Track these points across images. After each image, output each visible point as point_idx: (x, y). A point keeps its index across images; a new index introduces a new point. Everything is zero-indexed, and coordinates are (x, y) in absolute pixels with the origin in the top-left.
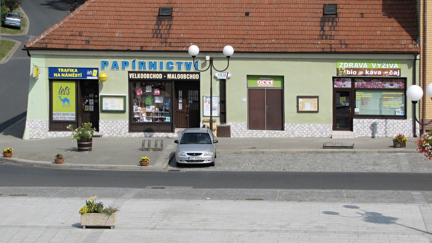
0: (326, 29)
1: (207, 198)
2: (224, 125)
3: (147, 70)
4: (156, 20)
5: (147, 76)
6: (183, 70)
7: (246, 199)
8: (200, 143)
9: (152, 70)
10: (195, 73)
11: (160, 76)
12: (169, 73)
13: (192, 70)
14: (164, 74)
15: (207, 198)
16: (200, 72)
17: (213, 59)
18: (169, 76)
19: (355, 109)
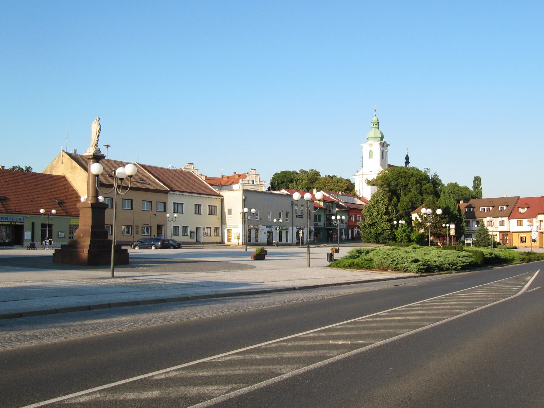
0: (249, 248)
1: (350, 230)
2: (33, 243)
3: (4, 220)
4: (306, 250)
5: (4, 223)
6: (19, 220)
7: (230, 245)
8: (271, 241)
9: (6, 220)
10: (23, 222)
11: (9, 223)
12: (13, 222)
13: (22, 221)
14: (11, 222)
15: (350, 230)
16: (256, 242)
17: (267, 244)
18: (13, 223)
19: (33, 171)
